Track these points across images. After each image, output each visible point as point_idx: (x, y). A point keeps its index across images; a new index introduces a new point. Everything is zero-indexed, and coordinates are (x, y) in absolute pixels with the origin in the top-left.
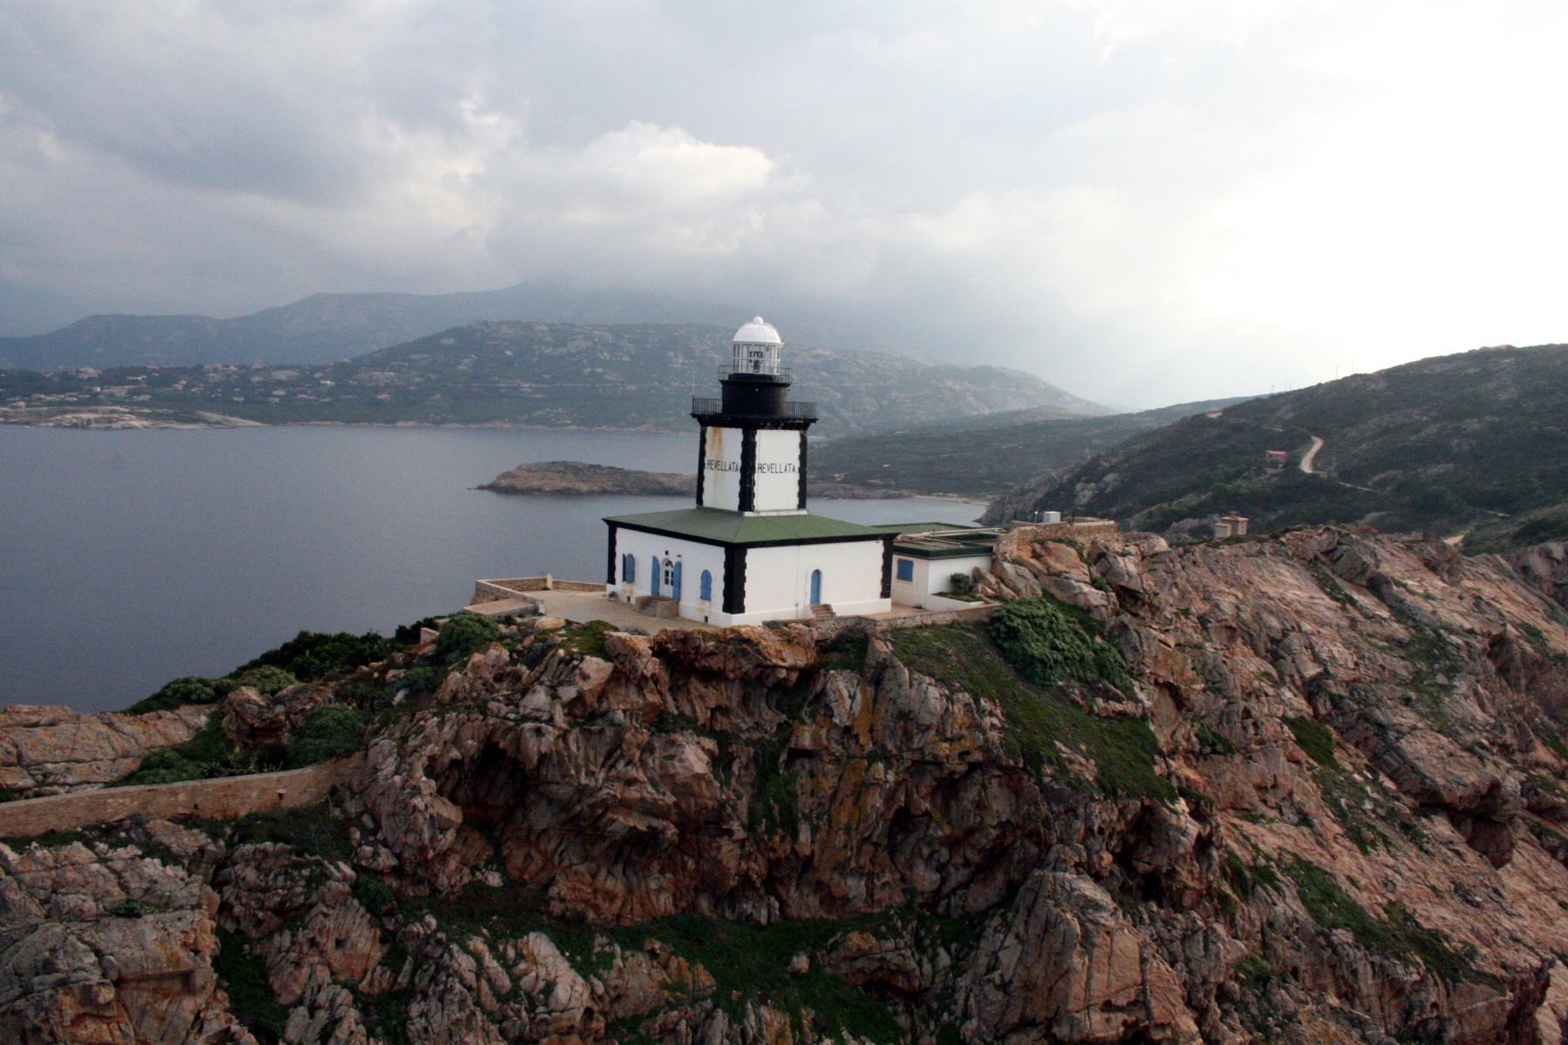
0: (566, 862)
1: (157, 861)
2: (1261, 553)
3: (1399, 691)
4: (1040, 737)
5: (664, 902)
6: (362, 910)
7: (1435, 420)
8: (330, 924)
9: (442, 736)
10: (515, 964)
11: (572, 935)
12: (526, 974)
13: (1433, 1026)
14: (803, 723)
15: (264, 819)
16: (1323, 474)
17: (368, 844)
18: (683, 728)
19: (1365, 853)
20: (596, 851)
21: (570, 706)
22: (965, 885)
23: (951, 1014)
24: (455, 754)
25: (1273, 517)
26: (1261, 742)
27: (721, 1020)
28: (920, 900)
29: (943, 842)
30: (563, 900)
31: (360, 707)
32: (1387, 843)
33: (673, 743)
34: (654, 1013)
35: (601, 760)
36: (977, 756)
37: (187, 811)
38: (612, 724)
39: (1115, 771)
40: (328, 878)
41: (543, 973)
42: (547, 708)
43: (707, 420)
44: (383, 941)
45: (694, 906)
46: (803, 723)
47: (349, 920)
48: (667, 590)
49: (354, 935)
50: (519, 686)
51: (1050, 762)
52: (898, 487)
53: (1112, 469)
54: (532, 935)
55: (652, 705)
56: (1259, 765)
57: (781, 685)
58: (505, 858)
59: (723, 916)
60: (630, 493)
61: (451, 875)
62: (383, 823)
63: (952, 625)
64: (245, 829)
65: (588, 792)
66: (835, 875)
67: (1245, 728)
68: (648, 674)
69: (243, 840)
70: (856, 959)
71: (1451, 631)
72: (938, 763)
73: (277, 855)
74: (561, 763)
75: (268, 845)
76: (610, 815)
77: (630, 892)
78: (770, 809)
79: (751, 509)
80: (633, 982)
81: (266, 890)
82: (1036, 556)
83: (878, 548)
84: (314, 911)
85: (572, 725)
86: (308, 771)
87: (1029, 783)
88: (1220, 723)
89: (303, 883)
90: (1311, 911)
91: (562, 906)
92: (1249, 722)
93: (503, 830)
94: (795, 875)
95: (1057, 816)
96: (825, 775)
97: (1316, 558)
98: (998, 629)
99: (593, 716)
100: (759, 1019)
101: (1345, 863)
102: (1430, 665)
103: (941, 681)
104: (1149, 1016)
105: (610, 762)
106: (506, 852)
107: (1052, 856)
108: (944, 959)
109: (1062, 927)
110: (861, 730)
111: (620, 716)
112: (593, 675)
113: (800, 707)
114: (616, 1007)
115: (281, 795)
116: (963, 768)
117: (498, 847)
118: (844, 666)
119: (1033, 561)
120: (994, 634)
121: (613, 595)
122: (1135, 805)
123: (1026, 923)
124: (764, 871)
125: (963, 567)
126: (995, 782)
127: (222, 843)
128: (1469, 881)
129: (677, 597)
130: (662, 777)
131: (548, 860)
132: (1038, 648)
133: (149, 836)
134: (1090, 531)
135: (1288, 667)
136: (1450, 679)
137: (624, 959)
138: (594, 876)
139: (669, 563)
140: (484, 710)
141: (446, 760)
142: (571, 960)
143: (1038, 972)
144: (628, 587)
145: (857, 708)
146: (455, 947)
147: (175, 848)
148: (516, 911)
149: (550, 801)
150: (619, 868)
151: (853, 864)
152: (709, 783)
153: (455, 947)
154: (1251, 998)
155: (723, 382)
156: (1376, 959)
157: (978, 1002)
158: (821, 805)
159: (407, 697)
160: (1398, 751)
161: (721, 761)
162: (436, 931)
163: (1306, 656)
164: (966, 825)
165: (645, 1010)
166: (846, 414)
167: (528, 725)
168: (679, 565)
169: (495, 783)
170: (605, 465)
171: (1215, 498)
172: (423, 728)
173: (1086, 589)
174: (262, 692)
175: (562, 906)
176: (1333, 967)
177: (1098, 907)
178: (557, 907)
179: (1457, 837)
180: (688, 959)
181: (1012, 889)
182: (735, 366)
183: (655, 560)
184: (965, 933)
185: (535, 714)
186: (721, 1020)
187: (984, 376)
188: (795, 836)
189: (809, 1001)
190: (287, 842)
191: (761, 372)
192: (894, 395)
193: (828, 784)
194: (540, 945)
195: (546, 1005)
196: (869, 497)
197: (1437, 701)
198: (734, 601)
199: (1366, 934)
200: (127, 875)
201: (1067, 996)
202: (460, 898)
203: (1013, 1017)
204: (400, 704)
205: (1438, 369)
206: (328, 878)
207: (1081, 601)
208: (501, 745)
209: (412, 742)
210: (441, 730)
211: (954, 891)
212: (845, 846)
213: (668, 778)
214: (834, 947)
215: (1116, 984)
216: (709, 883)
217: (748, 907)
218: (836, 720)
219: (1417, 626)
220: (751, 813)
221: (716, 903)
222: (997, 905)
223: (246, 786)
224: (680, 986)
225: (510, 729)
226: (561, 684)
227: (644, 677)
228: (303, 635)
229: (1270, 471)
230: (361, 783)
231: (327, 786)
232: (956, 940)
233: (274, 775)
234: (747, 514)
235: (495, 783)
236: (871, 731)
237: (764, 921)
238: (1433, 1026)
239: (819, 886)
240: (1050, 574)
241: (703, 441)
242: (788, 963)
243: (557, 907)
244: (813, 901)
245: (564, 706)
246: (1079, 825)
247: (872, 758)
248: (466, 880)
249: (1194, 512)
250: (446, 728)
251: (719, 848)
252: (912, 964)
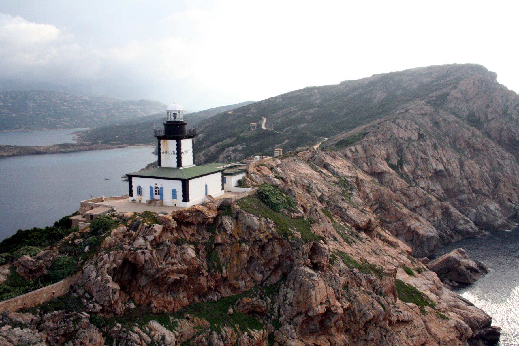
0: (154, 295)
1: (19, 328)
2: (295, 160)
3: (341, 197)
4: (285, 228)
5: (185, 301)
6: (95, 327)
7: (300, 110)
8: (87, 335)
9: (109, 260)
10: (150, 333)
11: (162, 318)
12: (154, 335)
13: (380, 290)
14: (217, 235)
15: (50, 303)
16: (270, 129)
17: (90, 303)
18: (184, 243)
19: (351, 246)
20: (163, 289)
21: (151, 242)
22: (270, 276)
23: (274, 316)
24: (115, 265)
25: (256, 144)
26: (321, 218)
27: (215, 335)
28: (258, 284)
29: (262, 265)
30: (156, 308)
31: (70, 255)
32: (354, 242)
33: (183, 248)
34: (194, 337)
35: (163, 258)
36: (270, 237)
37: (22, 307)
38: (167, 246)
39: (305, 234)
40: (81, 319)
41: (160, 334)
42: (144, 244)
43: (159, 138)
44: (103, 336)
45: (194, 300)
46: (217, 235)
47: (92, 332)
48: (157, 197)
49: (94, 337)
50: (131, 238)
51: (290, 234)
52: (122, 144)
53: (201, 132)
54: (151, 322)
55: (176, 237)
56: (322, 225)
57: (209, 224)
58: (133, 298)
59: (202, 301)
60: (24, 155)
61: (120, 308)
62: (94, 295)
63: (249, 196)
64: (45, 308)
65: (160, 270)
66: (235, 281)
67: (317, 215)
68: (174, 227)
69: (45, 312)
70: (245, 306)
71: (348, 178)
72: (260, 241)
73: (59, 315)
74: (151, 262)
75: (56, 312)
76: (168, 276)
77: (174, 300)
78: (214, 264)
79: (181, 166)
80: (186, 329)
81: (58, 328)
82: (258, 171)
83: (220, 174)
84: (79, 332)
85: (153, 248)
86: (62, 282)
87: (285, 242)
88: (310, 214)
89: (72, 323)
90: (347, 265)
91: (156, 310)
92: (317, 213)
93: (130, 289)
94: (222, 284)
95: (294, 250)
96: (227, 250)
97: (309, 160)
98: (262, 196)
99: (158, 245)
100: (225, 331)
101: (347, 249)
102: (345, 188)
103: (256, 215)
104: (330, 304)
105: (166, 258)
106: (133, 296)
107: (296, 263)
108: (269, 300)
109: (307, 283)
110: (235, 234)
111: (168, 243)
112: (158, 230)
113: (215, 230)
114: (182, 338)
115: (53, 293)
116: (267, 241)
117: (130, 295)
118: (226, 214)
119: (258, 173)
120: (261, 198)
121: (134, 200)
122: (312, 243)
123: (294, 284)
124: (214, 284)
125: (240, 177)
126: (276, 243)
127: (38, 315)
128: (375, 248)
129: (162, 199)
130: (181, 260)
131: (148, 296)
132: (274, 200)
133: (11, 320)
134: (267, 160)
135: (313, 195)
136: (351, 191)
137: (180, 322)
138: (163, 297)
139: (157, 187)
140: (122, 248)
141: (112, 268)
142: (165, 327)
143: (301, 298)
144: (139, 197)
145: (233, 228)
146: (130, 332)
147: (23, 322)
148: (143, 315)
149: (146, 275)
150: (169, 293)
151: (240, 277)
152: (196, 260)
153: (130, 332)
154: (345, 293)
155: (165, 124)
156: (365, 275)
157: (284, 311)
158: (227, 260)
159: (89, 248)
160: (347, 215)
161: (197, 251)
162: (122, 328)
163: (316, 190)
164: (269, 258)
165: (191, 337)
166: (96, 119)
167: (139, 251)
168: (162, 188)
169: (129, 272)
170: (12, 145)
171: (238, 140)
172: (102, 259)
173: (275, 179)
174: (31, 256)
175: (156, 310)
176: (355, 279)
177: (313, 275)
178: (154, 311)
179: (368, 237)
180: (199, 318)
181: (285, 276)
182: (168, 118)
183: (151, 187)
184: (274, 290)
185: (140, 247)
186: (215, 335)
187: (142, 103)
188: (222, 272)
189: (237, 322)
190: (62, 309)
191: (177, 120)
192: (113, 111)
193: (228, 252)
194: (154, 324)
195: (164, 343)
196: (113, 148)
197: (350, 198)
198: (186, 198)
199: (361, 269)
200: (9, 336)
201: (311, 303)
202: (124, 315)
203: (295, 313)
204: (88, 251)
205: (296, 94)
206: (81, 319)
207: (274, 183)
208: (130, 259)
209: (100, 264)
210: (109, 258)
211: (267, 279)
212: (237, 271)
213: (184, 260)
214: (238, 304)
215: (322, 297)
216: (200, 293)
217: (210, 297)
218: (228, 232)
219: (339, 177)
220: (208, 266)
221: (200, 298)
222: (280, 281)
223: (41, 292)
224: (199, 327)
225: (132, 254)
226: (147, 235)
227: (173, 228)
228: (20, 232)
229: (253, 129)
230: (82, 282)
231: (68, 286)
232: (271, 293)
233: (50, 286)
234: (181, 168)
235: (129, 272)
236: (238, 234)
237: (216, 300)
238: (380, 290)
239: (230, 285)
240: (264, 176)
241: (159, 145)
242: (227, 311)
243: (154, 311)
244: (229, 290)
245: (150, 242)
246: (301, 252)
247: (240, 243)
248: (124, 308)
249: (232, 145)
250: (111, 257)
251: (200, 280)
252: (262, 304)
